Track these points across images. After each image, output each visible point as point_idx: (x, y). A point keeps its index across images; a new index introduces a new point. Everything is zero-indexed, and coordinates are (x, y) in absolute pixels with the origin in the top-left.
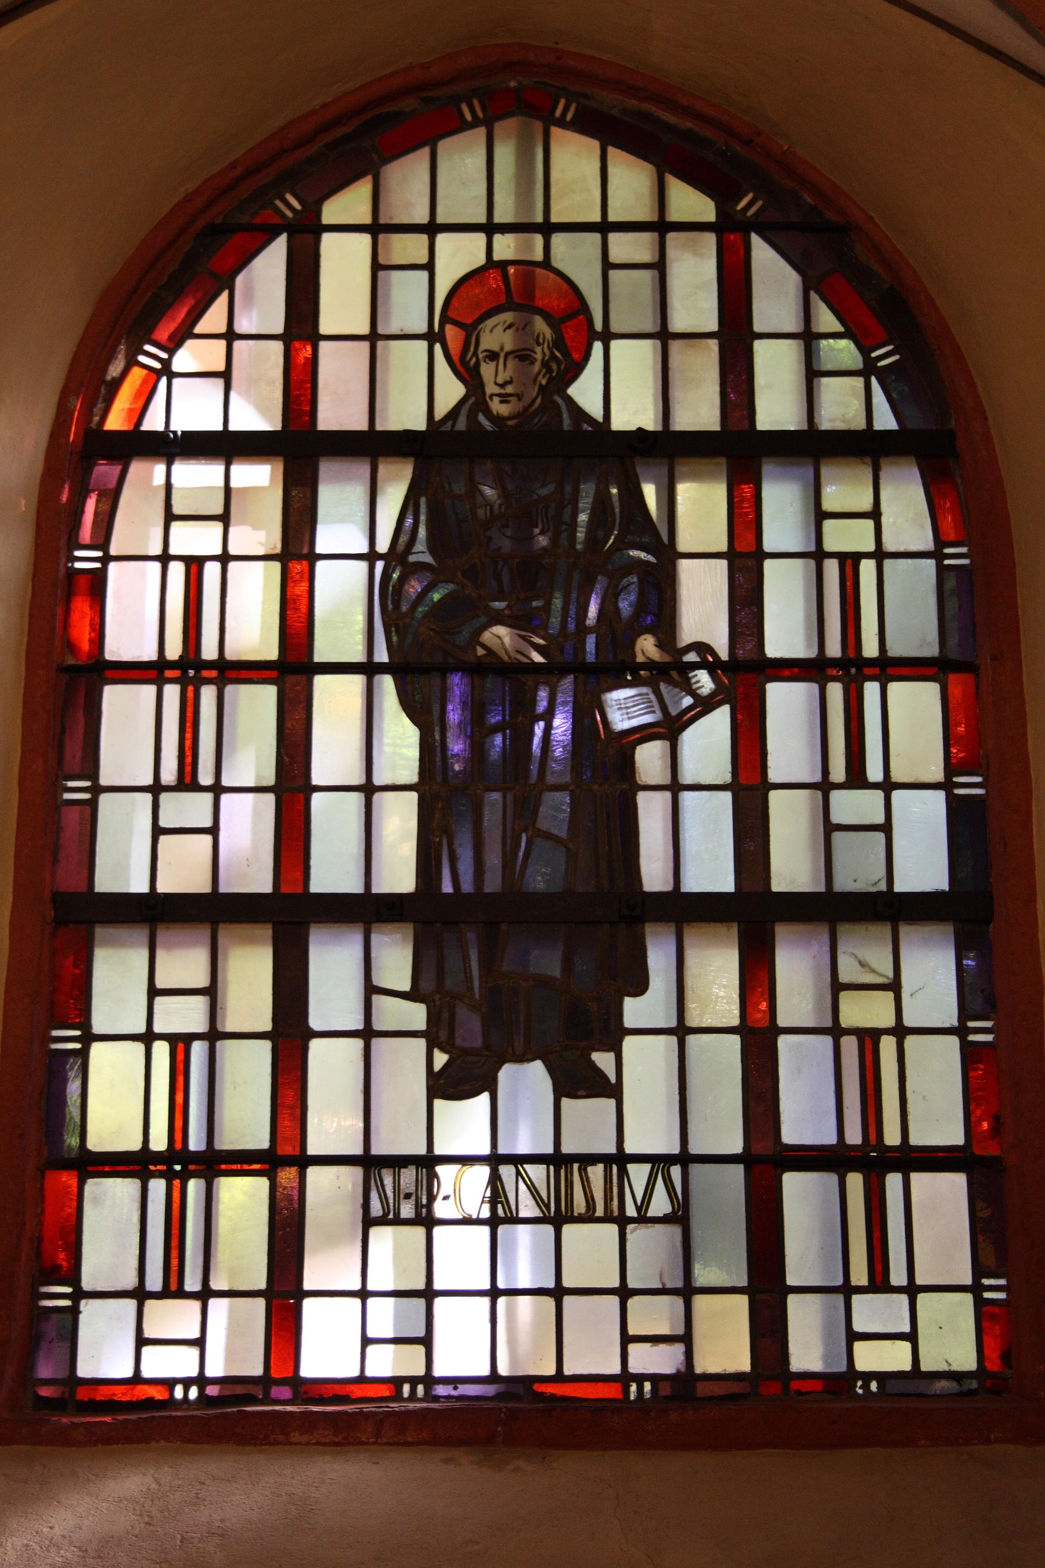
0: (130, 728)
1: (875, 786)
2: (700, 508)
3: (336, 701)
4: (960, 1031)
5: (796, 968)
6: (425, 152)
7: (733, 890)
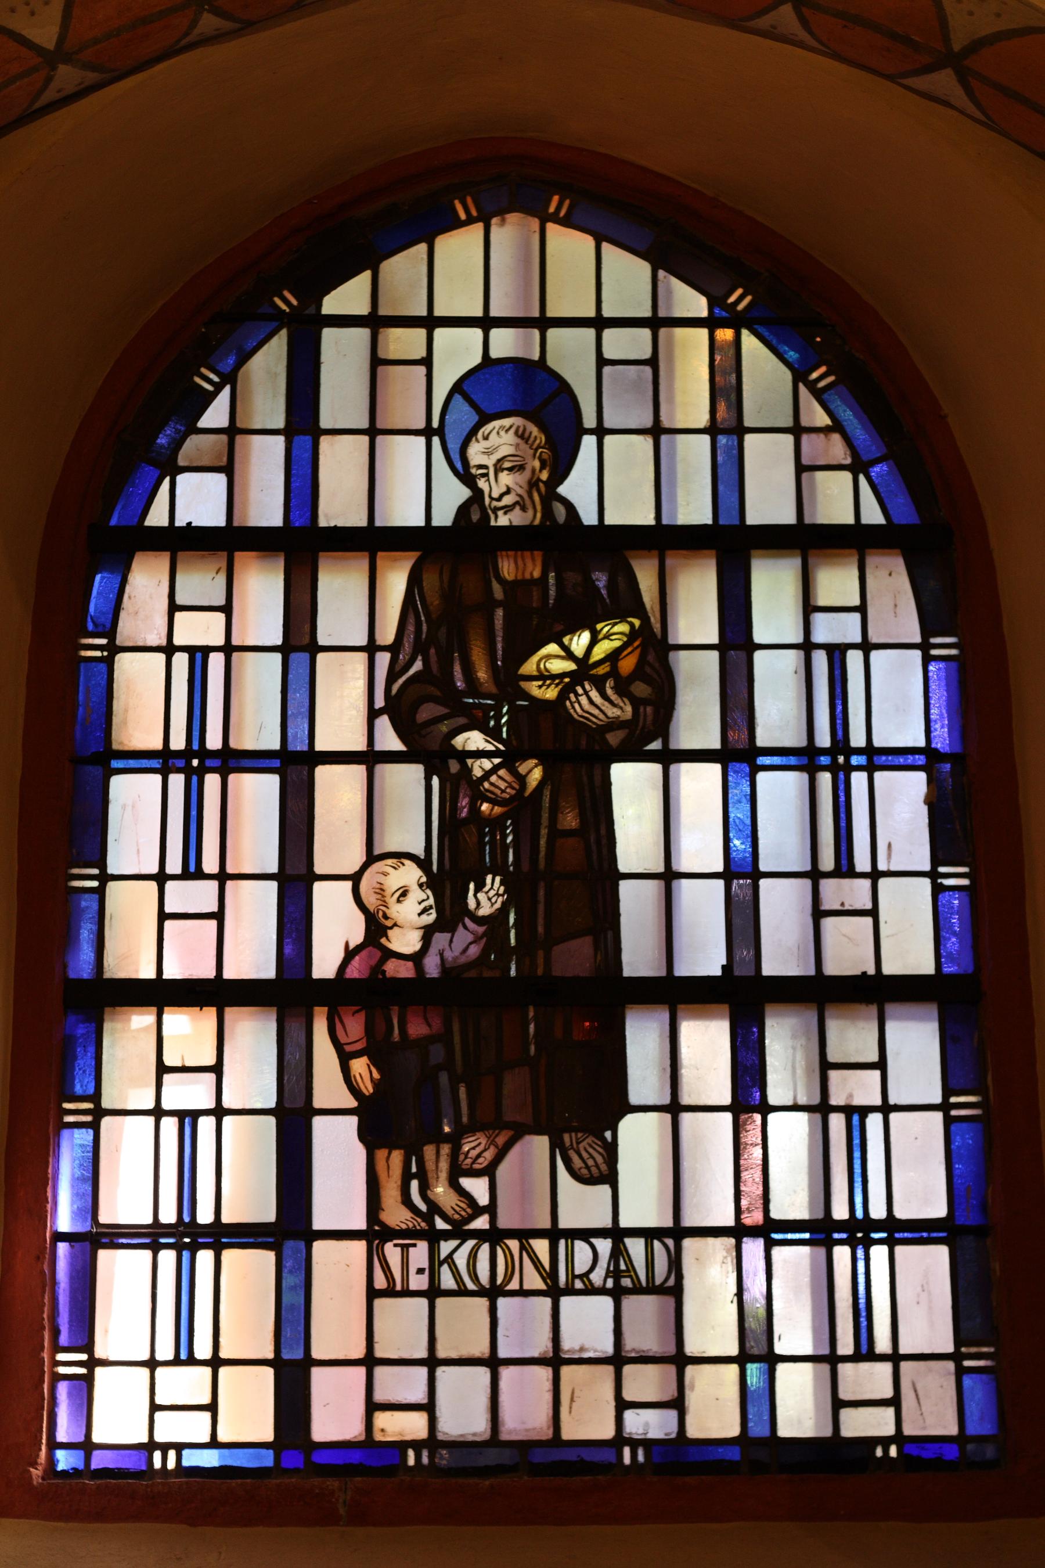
0: (137, 812)
1: (863, 875)
3: (338, 791)
4: (944, 1107)
5: (783, 1042)
6: (423, 247)
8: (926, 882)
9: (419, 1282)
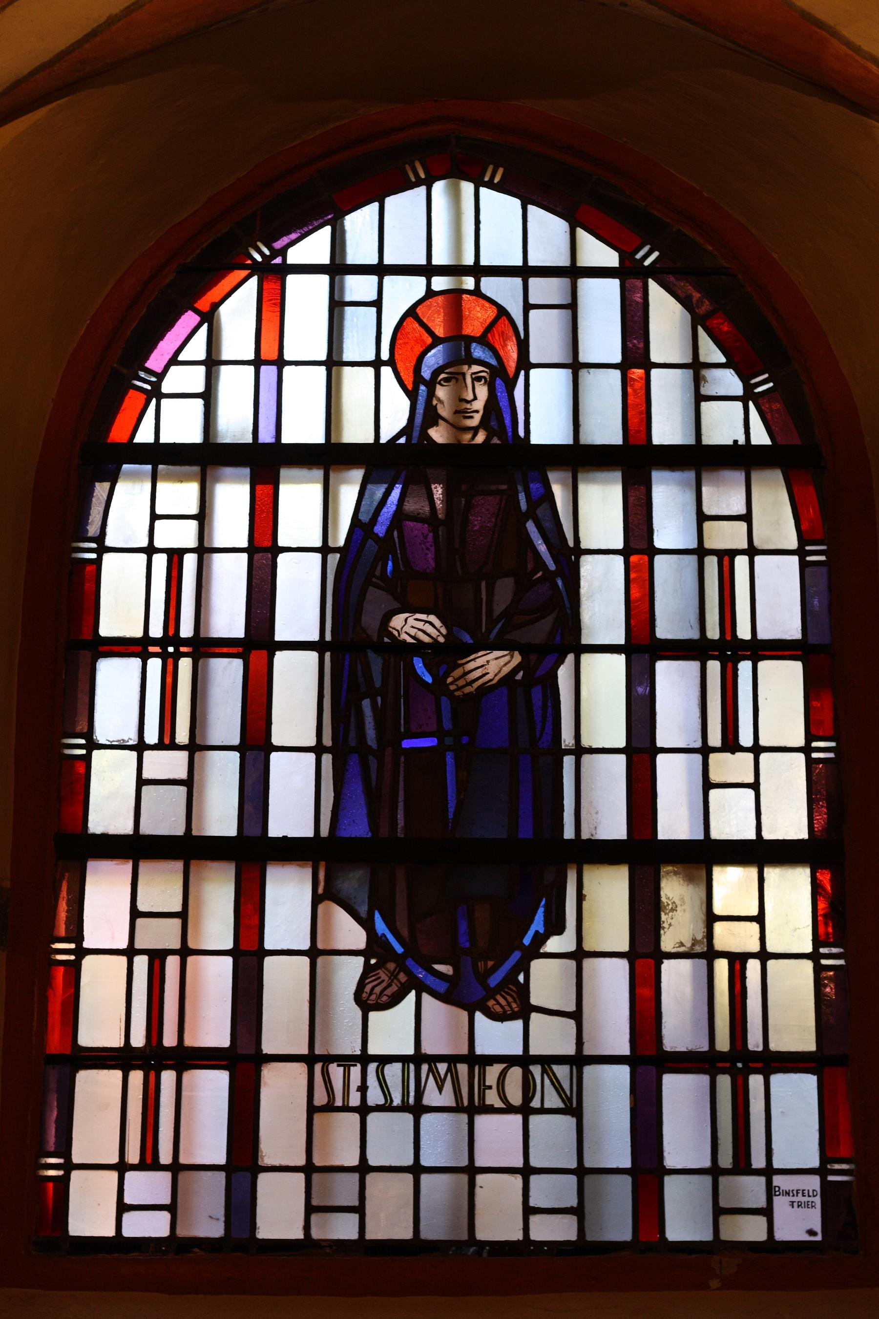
0: (118, 694)
2: (600, 512)
4: (806, 750)
5: (668, 497)
6: (375, 206)
7: (625, 838)
8: (801, 757)
9: (355, 1100)
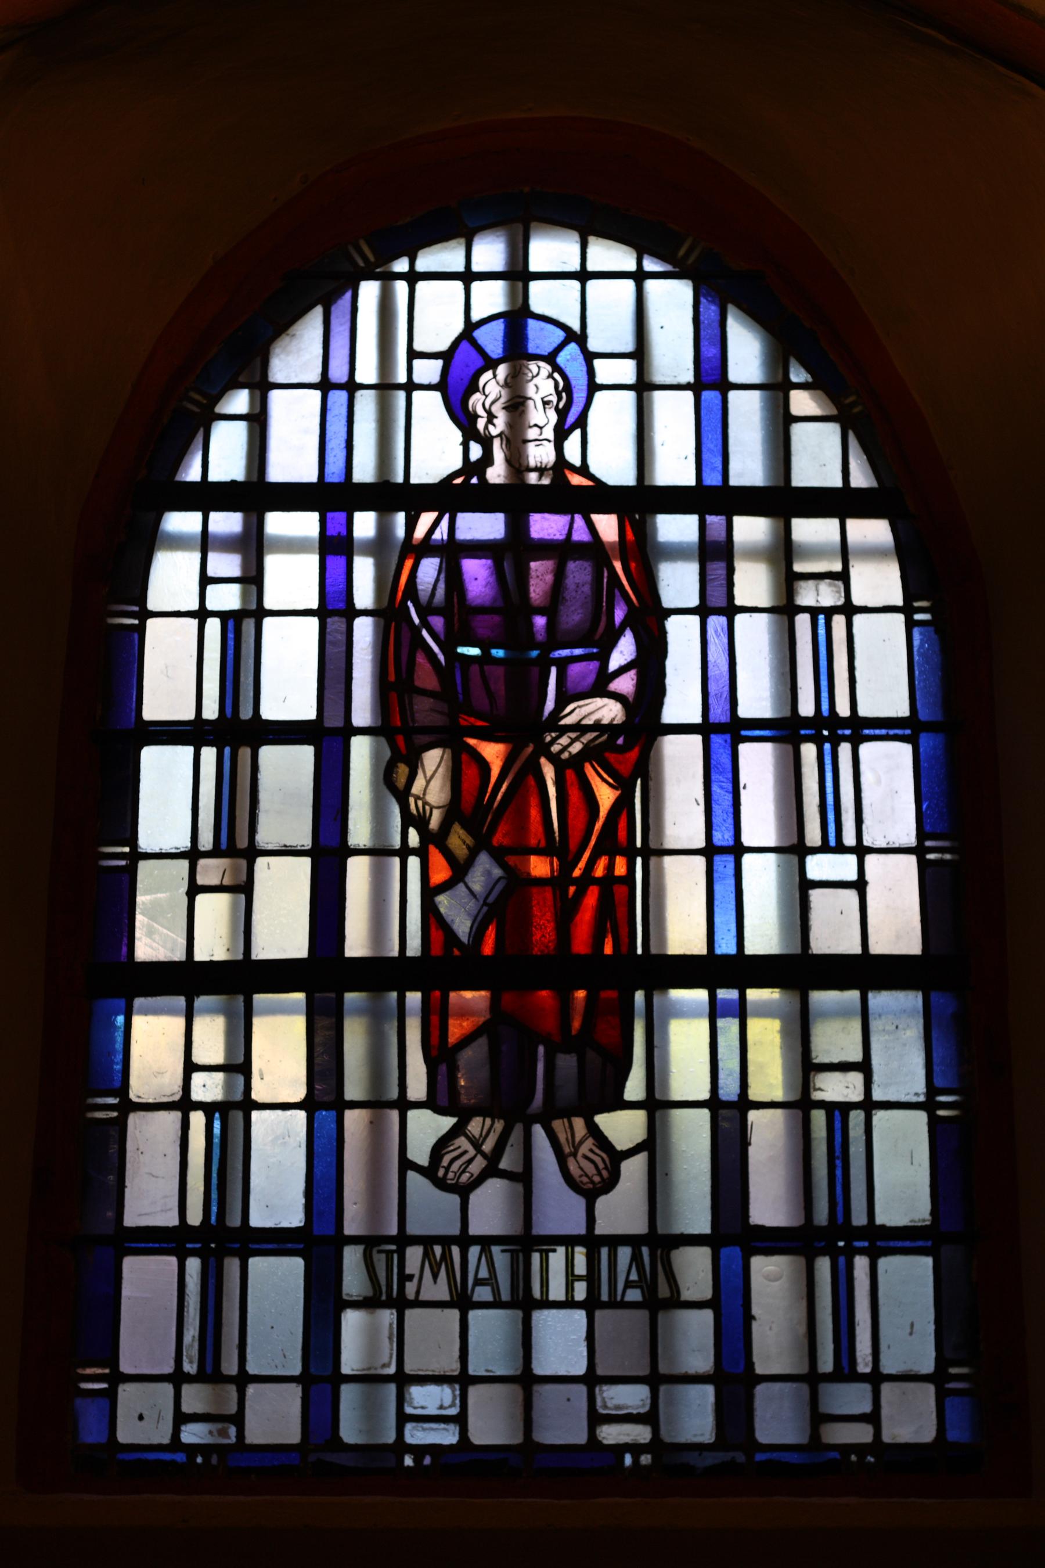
1: (863, 1378)
